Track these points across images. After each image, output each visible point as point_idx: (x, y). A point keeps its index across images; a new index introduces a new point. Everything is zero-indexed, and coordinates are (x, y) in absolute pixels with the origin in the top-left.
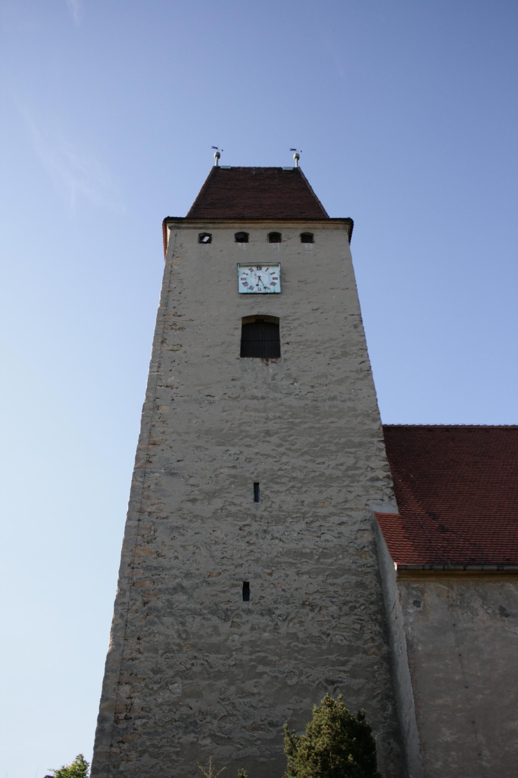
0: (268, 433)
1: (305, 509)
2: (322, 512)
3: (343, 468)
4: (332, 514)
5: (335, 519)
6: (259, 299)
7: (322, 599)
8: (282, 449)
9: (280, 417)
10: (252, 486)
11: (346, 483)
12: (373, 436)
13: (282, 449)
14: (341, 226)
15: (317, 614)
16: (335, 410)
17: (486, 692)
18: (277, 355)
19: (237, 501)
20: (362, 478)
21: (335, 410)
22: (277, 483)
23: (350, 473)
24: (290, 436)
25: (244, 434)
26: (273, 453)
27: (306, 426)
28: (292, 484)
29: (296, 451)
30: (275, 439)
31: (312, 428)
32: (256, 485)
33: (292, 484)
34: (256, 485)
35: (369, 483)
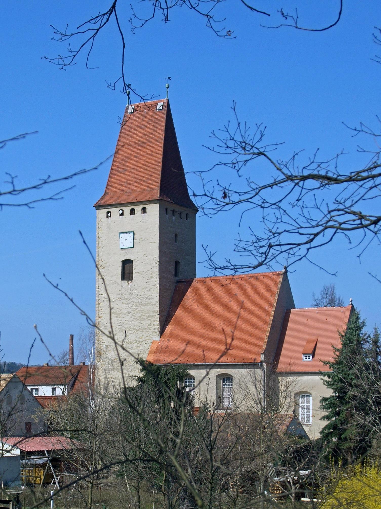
0: (129, 313)
1: (137, 339)
2: (141, 340)
3: (147, 325)
4: (144, 341)
5: (144, 343)
6: (127, 250)
7: (107, 341)
8: (132, 319)
9: (132, 306)
10: (124, 332)
11: (148, 330)
12: (156, 313)
13: (132, 319)
14: (156, 202)
15: (323, 479)
16: (147, 303)
17: (265, 492)
18: (132, 279)
19: (120, 337)
20: (152, 329)
21: (147, 303)
22: (131, 331)
23: (149, 327)
24: (134, 313)
25: (122, 313)
26: (129, 320)
27: (138, 309)
28: (134, 331)
29: (136, 319)
30: (130, 315)
31: (140, 310)
32: (125, 331)
33: (134, 331)
34: (125, 331)
35: (153, 330)
